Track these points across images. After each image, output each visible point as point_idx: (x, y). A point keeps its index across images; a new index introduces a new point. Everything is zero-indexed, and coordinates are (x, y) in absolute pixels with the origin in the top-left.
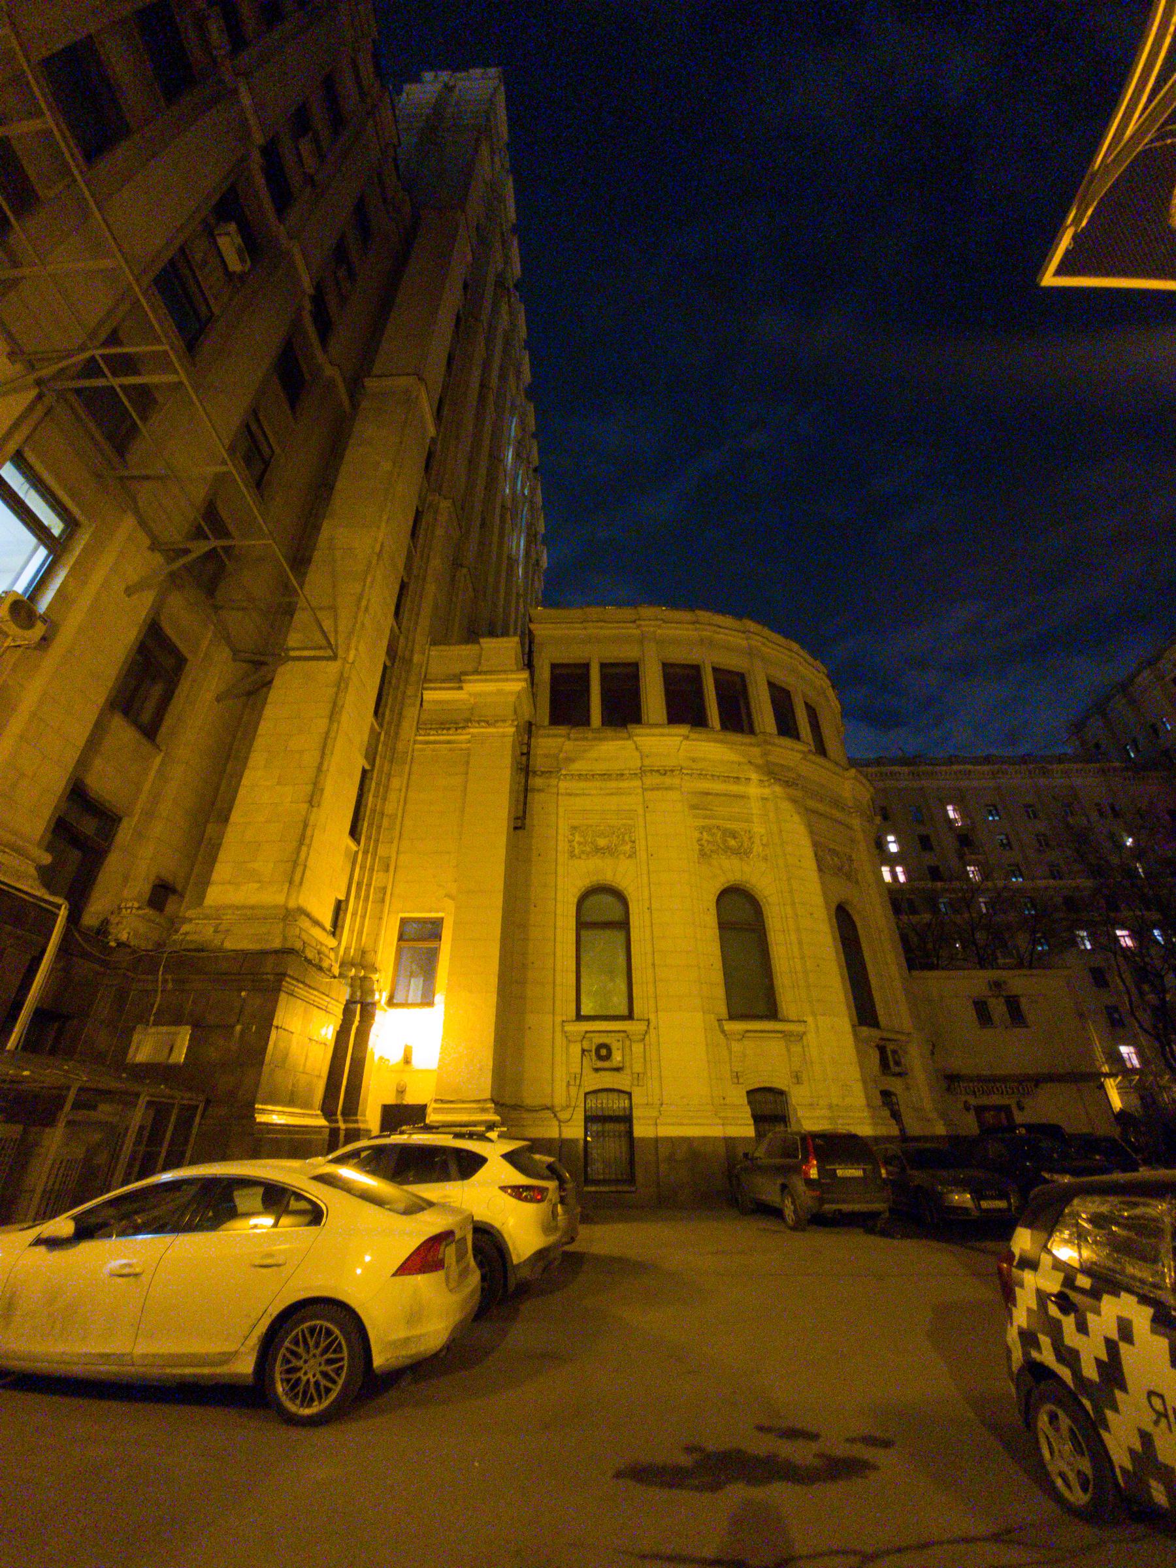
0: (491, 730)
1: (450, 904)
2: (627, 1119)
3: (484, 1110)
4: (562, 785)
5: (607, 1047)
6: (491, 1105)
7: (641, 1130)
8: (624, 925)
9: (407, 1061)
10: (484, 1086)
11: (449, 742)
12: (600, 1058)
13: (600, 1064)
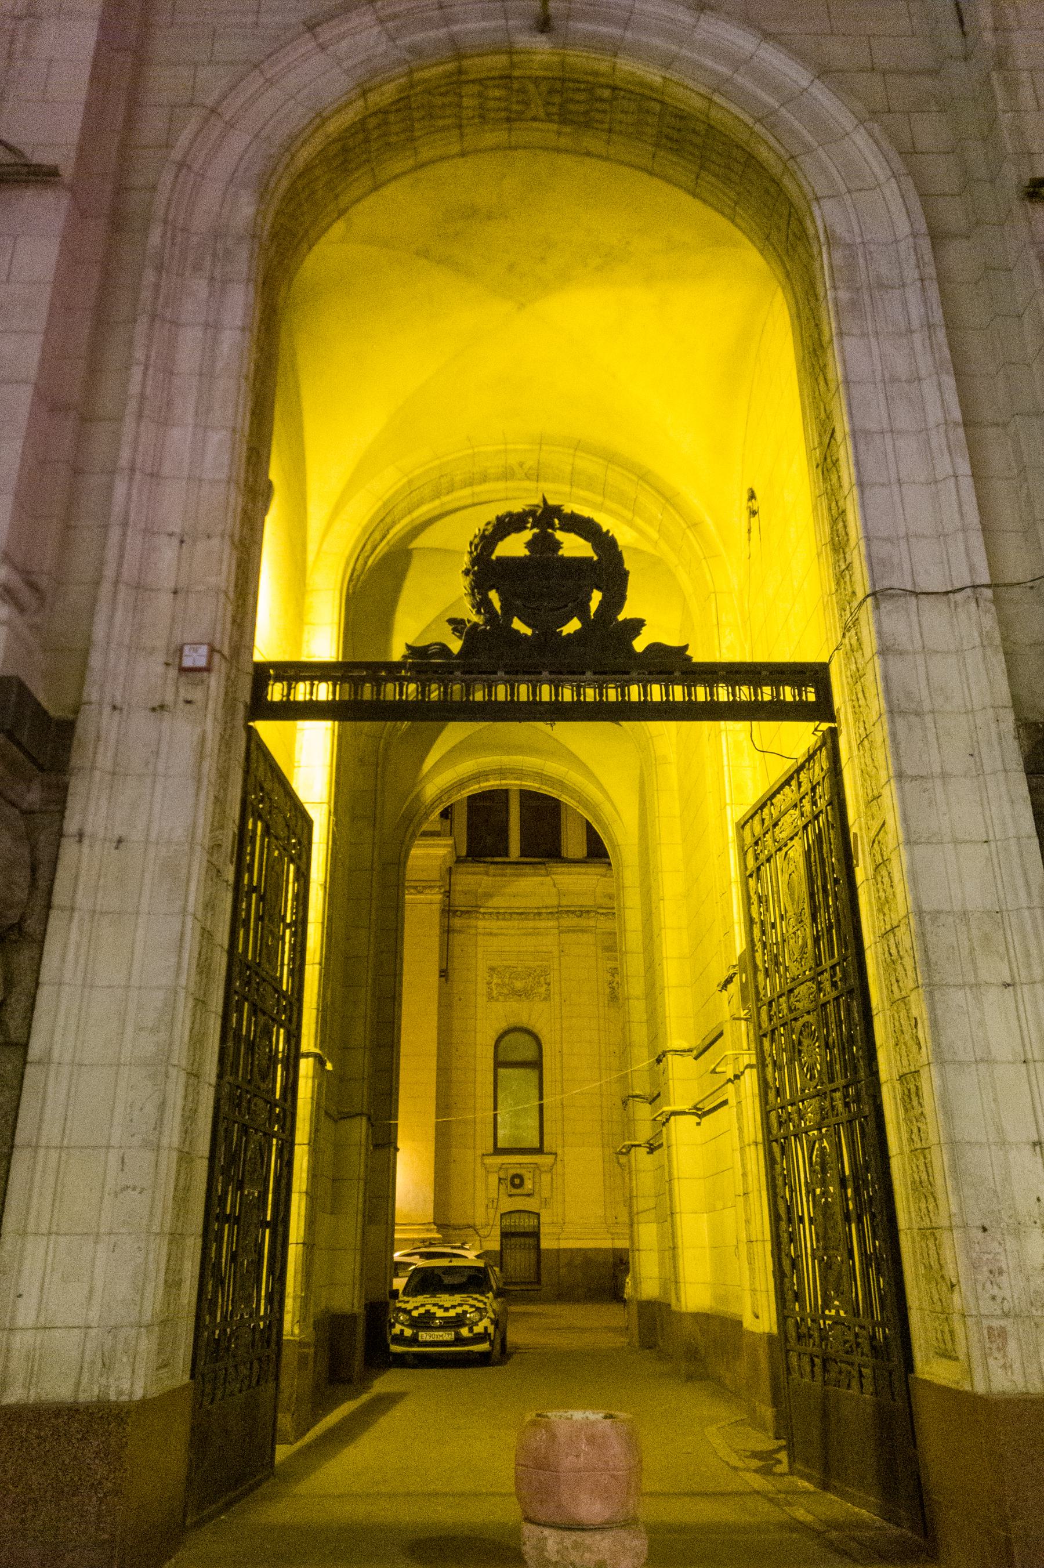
3: (429, 1231)
4: (481, 924)
6: (433, 1227)
7: (545, 1245)
8: (536, 1064)
12: (514, 1186)
13: (514, 1191)
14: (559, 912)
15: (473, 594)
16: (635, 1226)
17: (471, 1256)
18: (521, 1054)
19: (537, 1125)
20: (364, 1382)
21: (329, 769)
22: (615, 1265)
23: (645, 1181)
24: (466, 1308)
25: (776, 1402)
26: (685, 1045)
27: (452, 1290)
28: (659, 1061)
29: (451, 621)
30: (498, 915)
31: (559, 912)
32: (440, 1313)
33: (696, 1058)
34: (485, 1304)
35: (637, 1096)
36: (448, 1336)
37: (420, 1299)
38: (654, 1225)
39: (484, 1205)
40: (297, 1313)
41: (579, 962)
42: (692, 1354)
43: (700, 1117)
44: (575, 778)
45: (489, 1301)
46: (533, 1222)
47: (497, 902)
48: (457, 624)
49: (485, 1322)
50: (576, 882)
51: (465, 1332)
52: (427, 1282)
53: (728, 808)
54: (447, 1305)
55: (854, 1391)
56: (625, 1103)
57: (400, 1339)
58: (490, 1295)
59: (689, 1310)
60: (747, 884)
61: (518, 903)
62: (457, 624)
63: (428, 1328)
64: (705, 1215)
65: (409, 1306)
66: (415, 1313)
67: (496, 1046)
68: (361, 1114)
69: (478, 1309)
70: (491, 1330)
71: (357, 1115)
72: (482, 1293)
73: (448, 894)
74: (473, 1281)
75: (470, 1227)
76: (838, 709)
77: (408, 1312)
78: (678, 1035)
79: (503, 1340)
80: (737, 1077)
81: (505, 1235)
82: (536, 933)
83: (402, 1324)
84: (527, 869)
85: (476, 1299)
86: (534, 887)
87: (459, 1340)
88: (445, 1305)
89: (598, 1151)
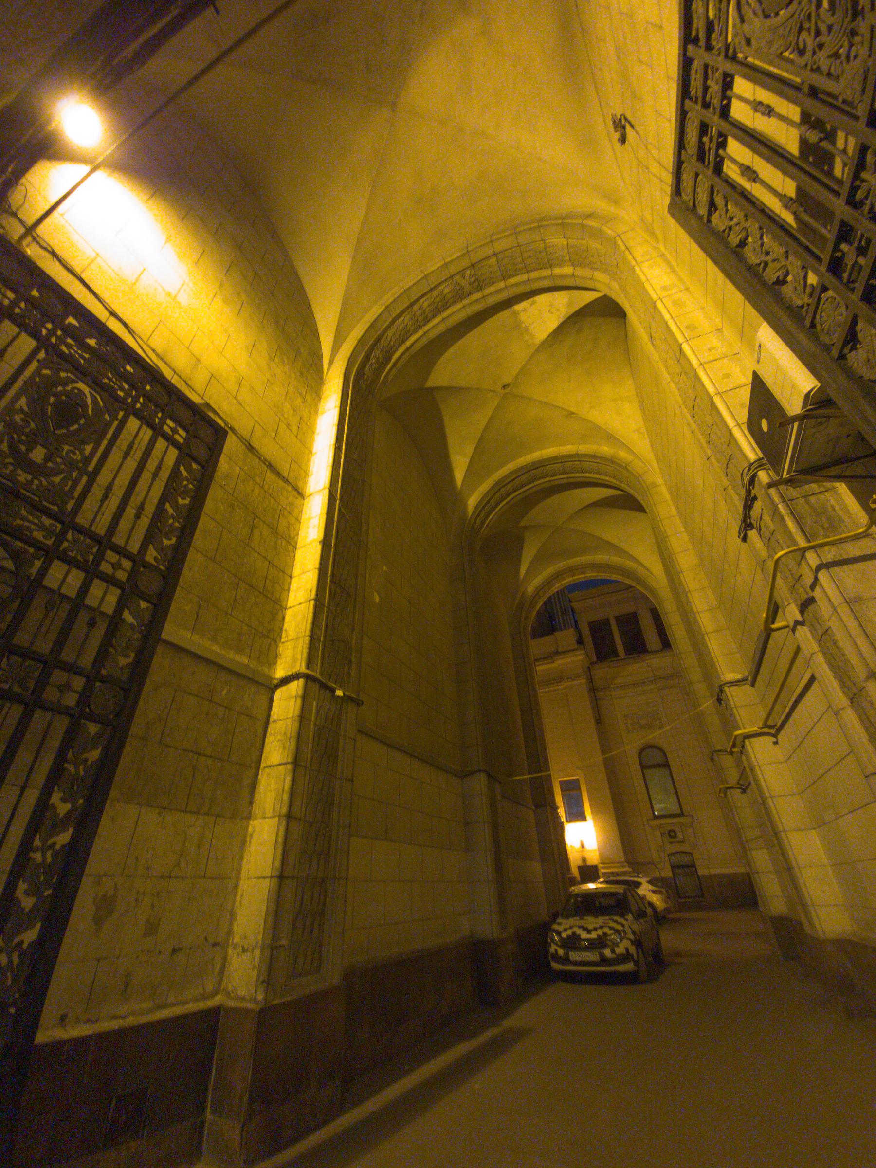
0: (574, 682)
1: (579, 772)
2: (693, 866)
3: (623, 867)
4: (614, 693)
5: (674, 832)
6: (626, 864)
7: (701, 871)
8: (666, 765)
9: (583, 846)
10: (621, 856)
11: (555, 690)
12: (671, 837)
13: (672, 840)
16: (749, 853)
19: (676, 800)
23: (746, 814)
24: (606, 930)
26: (739, 676)
33: (753, 685)
34: (623, 926)
35: (720, 751)
36: (592, 956)
38: (765, 851)
43: (774, 736)
49: (626, 943)
50: (657, 662)
51: (607, 952)
52: (590, 905)
54: (590, 927)
56: (712, 759)
57: (556, 958)
58: (630, 917)
63: (576, 948)
64: (813, 831)
66: (564, 935)
68: (480, 771)
69: (617, 931)
70: (633, 950)
71: (476, 772)
72: (622, 916)
73: (591, 680)
75: (650, 863)
77: (559, 933)
81: (673, 867)
83: (556, 944)
85: (616, 922)
86: (637, 669)
87: (604, 961)
88: (589, 928)
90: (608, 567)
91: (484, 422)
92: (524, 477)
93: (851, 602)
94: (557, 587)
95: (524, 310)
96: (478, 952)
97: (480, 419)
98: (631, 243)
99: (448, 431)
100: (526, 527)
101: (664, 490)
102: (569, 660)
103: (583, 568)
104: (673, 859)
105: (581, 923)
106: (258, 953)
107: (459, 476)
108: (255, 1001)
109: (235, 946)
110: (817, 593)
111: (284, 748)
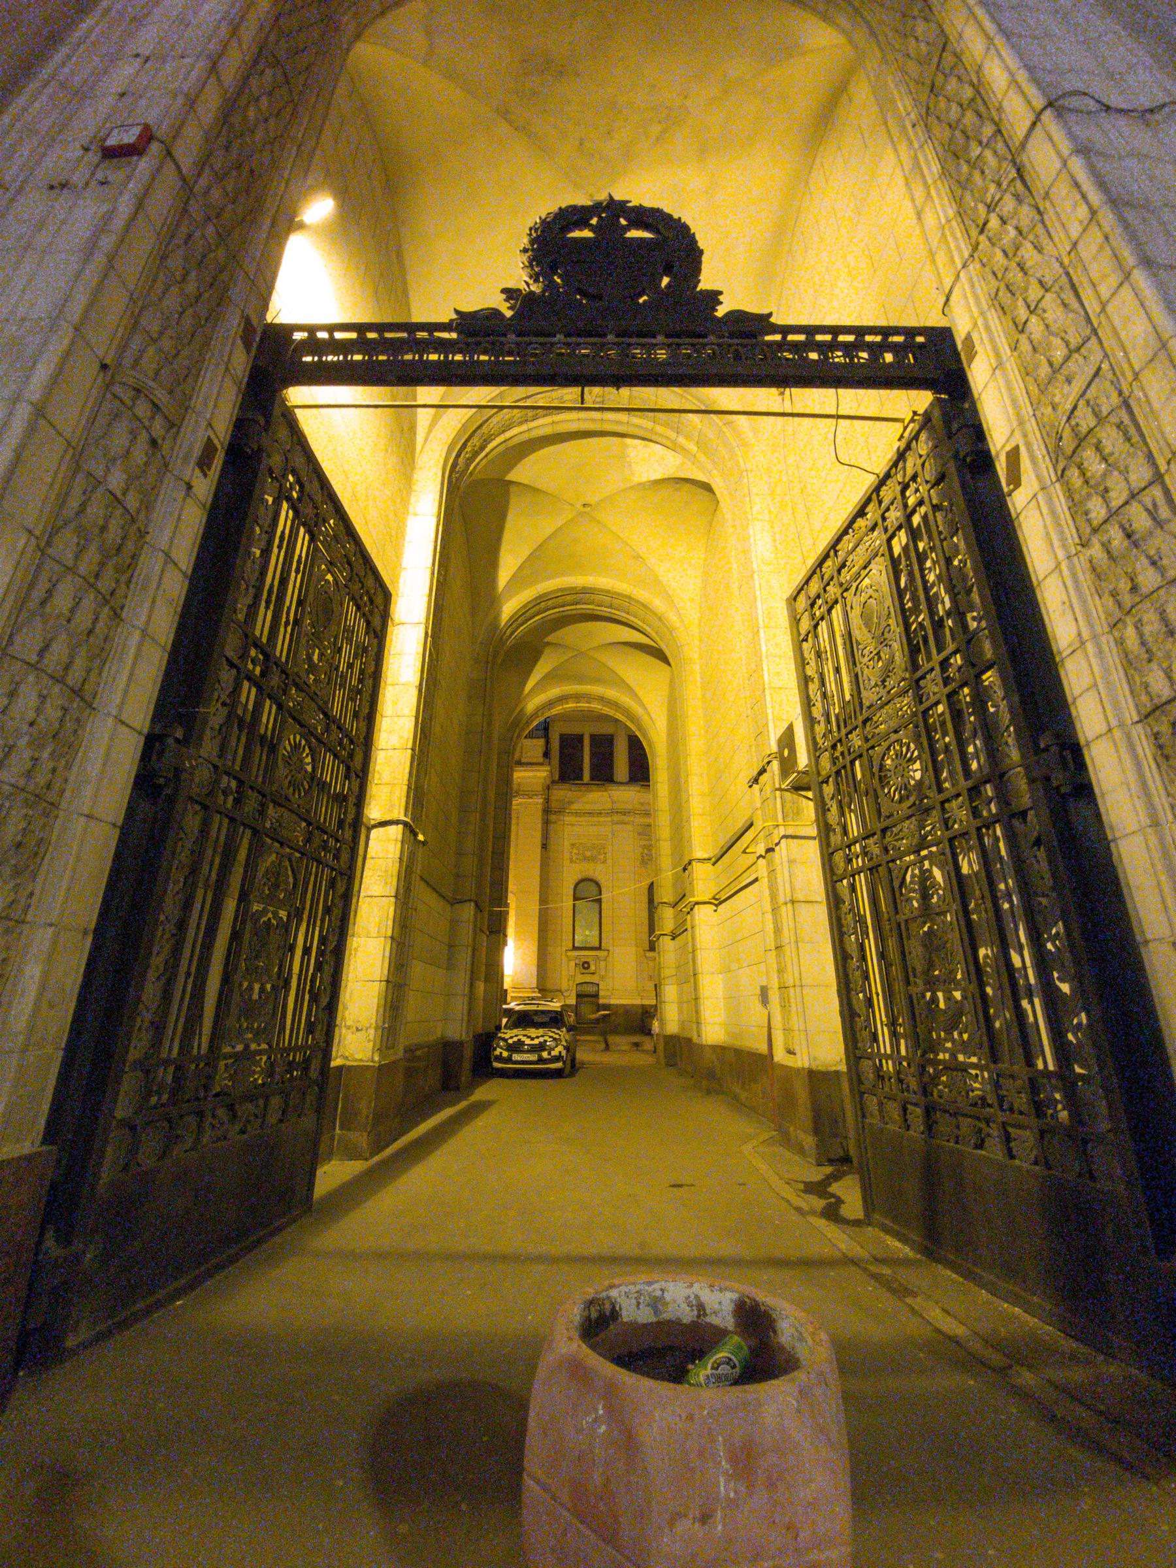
4: (567, 819)
14: (614, 812)
15: (531, 266)
17: (555, 1005)
18: (588, 891)
20: (472, 1086)
21: (426, 599)
22: (643, 1014)
24: (546, 1038)
25: (816, 1131)
26: (706, 856)
27: (538, 1025)
28: (685, 869)
29: (504, 291)
30: (577, 814)
31: (614, 812)
32: (528, 1041)
36: (533, 1057)
37: (515, 1031)
39: (567, 978)
40: (378, 1041)
41: (624, 844)
42: (711, 1075)
43: (716, 905)
44: (625, 700)
45: (563, 1034)
46: (595, 988)
47: (575, 807)
48: (510, 293)
49: (560, 1048)
51: (545, 1054)
52: (524, 1020)
53: (762, 632)
55: (994, 1150)
57: (499, 1059)
59: (709, 1043)
60: (801, 649)
61: (588, 807)
62: (510, 293)
65: (507, 1036)
66: (510, 1041)
67: (575, 887)
68: (470, 900)
69: (555, 1039)
70: (564, 1053)
72: (559, 1029)
73: (547, 801)
74: (554, 1020)
76: (968, 338)
77: (505, 1040)
78: (701, 845)
79: (573, 1060)
80: (770, 850)
82: (599, 824)
84: (594, 787)
86: (598, 798)
87: (541, 1060)
88: (532, 1036)
89: (633, 949)
90: (615, 705)
91: (548, 531)
92: (568, 598)
93: (791, 862)
94: (557, 710)
95: (635, 447)
96: (448, 1049)
97: (547, 526)
98: (754, 491)
99: (509, 524)
100: (548, 644)
101: (697, 667)
102: (530, 774)
103: (588, 697)
104: (579, 988)
105: (524, 1032)
106: (372, 1031)
107: (504, 576)
108: (373, 1061)
109: (348, 1028)
110: (777, 849)
111: (386, 883)
